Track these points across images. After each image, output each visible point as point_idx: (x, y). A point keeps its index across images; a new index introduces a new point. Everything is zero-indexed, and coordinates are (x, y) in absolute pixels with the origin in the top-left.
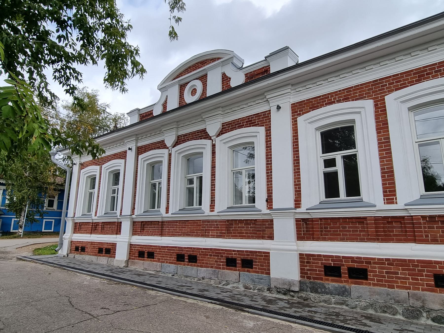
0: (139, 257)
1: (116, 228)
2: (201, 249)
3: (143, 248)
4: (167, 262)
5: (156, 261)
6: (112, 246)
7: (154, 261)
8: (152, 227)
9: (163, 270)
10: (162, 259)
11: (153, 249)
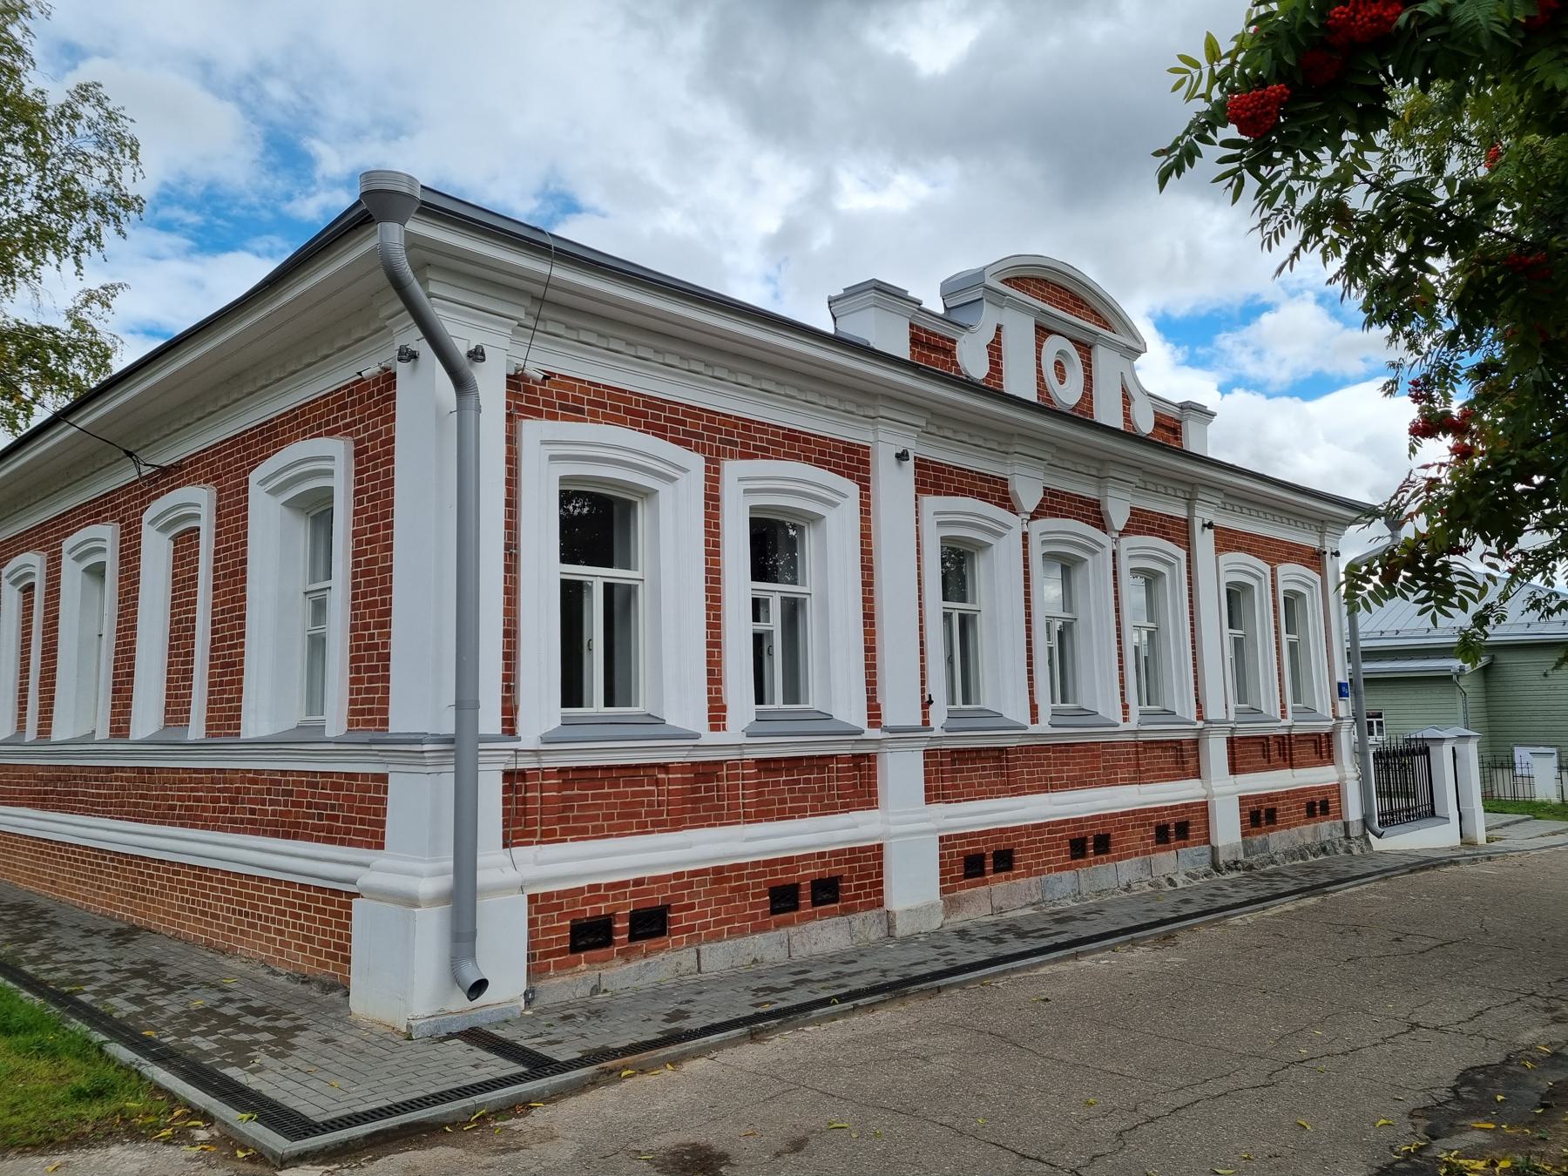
0: (966, 876)
1: (854, 780)
2: (1116, 815)
3: (977, 843)
4: (1050, 870)
5: (1022, 875)
6: (847, 861)
7: (1016, 877)
8: (977, 770)
9: (1048, 897)
10: (1038, 864)
11: (1008, 839)
